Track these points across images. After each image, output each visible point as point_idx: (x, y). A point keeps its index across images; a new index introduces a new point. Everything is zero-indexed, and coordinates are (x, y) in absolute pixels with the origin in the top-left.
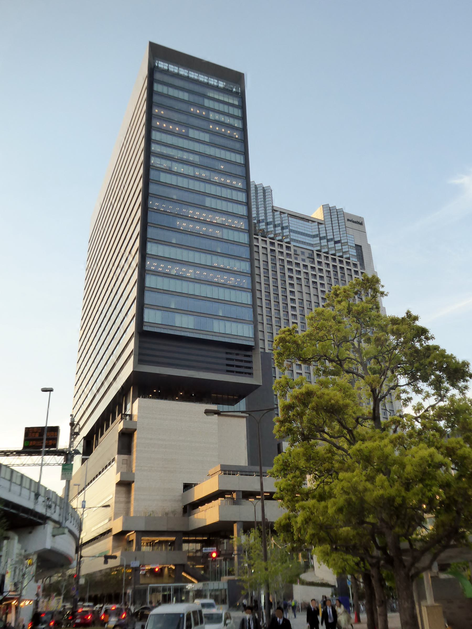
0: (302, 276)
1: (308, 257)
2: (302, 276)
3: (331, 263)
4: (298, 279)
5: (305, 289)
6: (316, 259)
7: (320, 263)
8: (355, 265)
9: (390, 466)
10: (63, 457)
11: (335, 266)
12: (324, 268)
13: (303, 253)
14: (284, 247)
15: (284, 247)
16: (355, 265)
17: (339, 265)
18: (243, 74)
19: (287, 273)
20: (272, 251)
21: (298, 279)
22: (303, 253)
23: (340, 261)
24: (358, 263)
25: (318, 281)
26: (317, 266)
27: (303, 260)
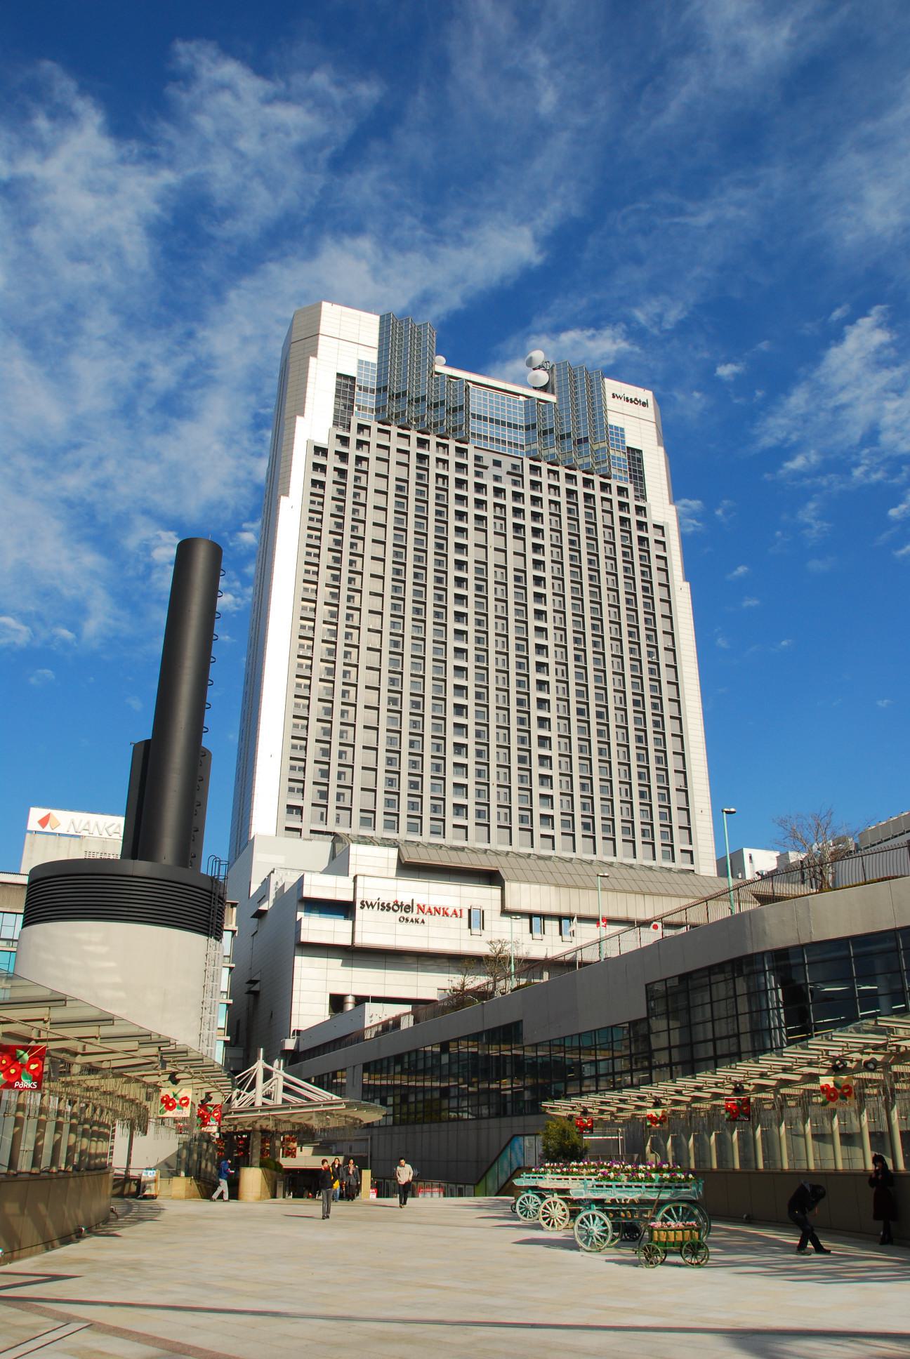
0: (489, 513)
1: (509, 473)
2: (489, 513)
3: (563, 485)
4: (479, 518)
5: (493, 541)
6: (528, 477)
7: (535, 485)
8: (621, 491)
9: (119, 254)
10: (326, 306)
11: (570, 493)
12: (546, 496)
13: (497, 464)
14: (562, 477)
15: (562, 477)
16: (621, 491)
17: (581, 490)
18: (136, 746)
19: (453, 506)
20: (624, 521)
21: (479, 518)
22: (497, 464)
23: (569, 477)
24: (630, 487)
25: (529, 523)
26: (528, 492)
27: (497, 478)
